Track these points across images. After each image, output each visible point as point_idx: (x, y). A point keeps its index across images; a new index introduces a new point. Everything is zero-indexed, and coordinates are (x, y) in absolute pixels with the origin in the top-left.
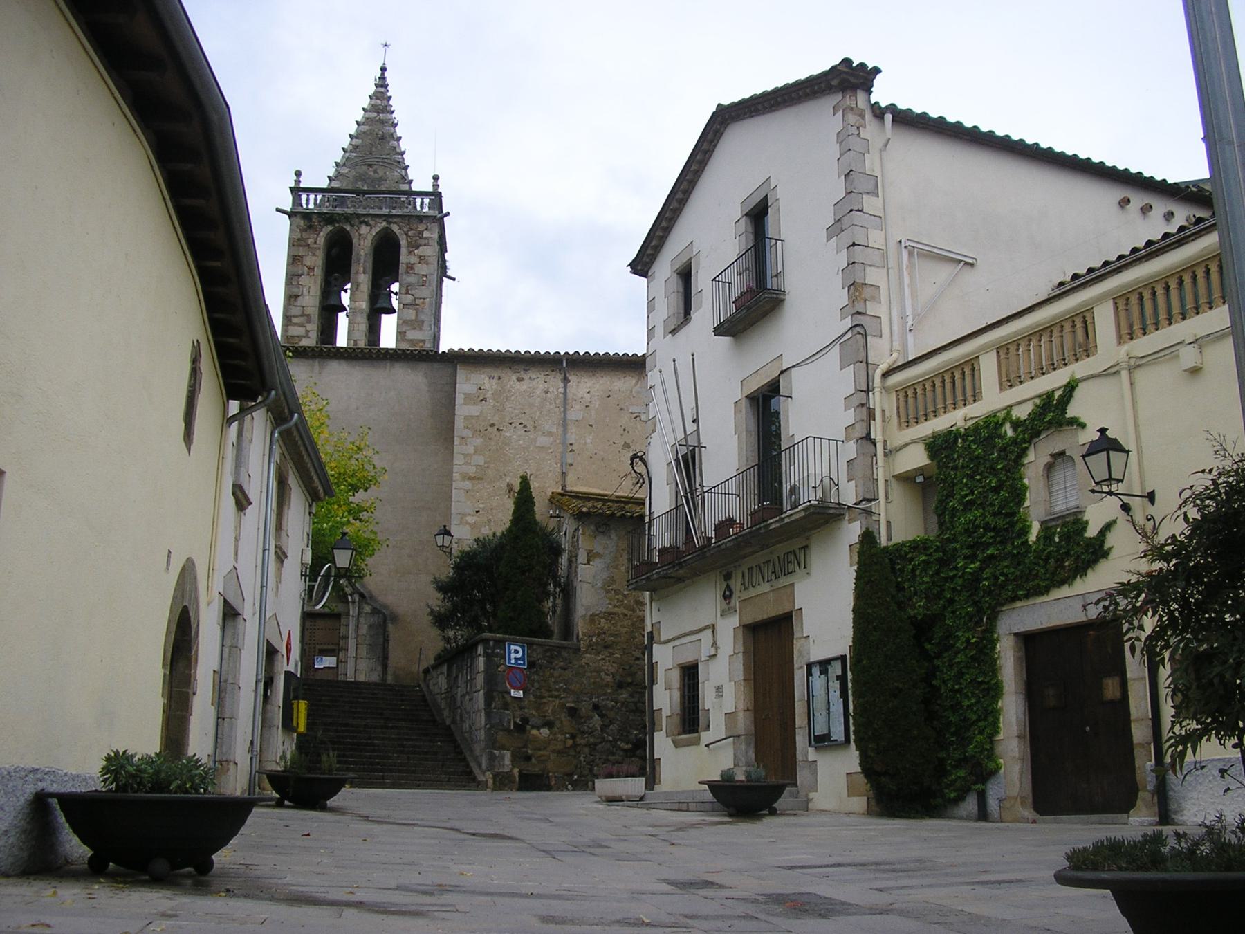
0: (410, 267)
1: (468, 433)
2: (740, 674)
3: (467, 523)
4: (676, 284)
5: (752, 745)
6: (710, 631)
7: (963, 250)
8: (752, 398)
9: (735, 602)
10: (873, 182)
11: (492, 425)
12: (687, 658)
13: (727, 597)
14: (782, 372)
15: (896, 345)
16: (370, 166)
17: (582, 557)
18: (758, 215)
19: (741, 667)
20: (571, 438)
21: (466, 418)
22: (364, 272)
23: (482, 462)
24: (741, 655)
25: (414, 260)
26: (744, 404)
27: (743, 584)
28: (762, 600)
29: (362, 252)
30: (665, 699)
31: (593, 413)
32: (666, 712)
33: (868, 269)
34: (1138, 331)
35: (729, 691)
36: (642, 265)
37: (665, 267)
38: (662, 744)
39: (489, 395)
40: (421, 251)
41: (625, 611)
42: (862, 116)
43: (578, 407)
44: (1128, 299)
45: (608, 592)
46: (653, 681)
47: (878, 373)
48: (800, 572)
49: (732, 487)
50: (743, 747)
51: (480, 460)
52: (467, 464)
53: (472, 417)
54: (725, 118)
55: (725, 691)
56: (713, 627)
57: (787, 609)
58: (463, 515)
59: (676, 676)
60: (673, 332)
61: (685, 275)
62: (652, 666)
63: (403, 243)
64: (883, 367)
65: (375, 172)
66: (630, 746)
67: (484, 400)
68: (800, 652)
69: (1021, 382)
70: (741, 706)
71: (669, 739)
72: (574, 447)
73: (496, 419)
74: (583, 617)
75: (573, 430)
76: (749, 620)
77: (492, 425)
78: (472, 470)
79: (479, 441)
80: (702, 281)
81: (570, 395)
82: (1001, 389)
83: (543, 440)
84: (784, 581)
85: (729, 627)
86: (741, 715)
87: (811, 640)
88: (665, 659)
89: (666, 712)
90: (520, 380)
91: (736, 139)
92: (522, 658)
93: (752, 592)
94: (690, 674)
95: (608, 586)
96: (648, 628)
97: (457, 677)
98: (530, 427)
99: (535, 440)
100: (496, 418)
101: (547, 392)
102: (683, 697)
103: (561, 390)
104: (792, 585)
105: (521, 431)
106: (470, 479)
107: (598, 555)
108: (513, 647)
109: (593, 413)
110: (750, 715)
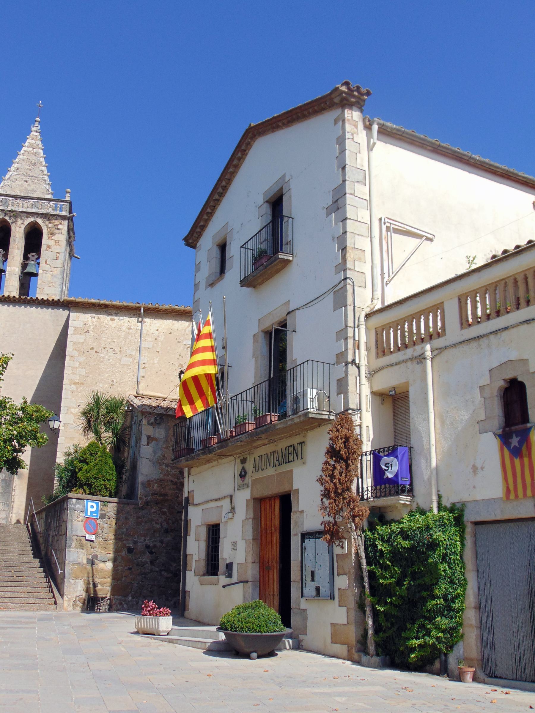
0: (49, 247)
1: (76, 353)
2: (250, 535)
3: (72, 413)
4: (216, 253)
5: (258, 589)
6: (228, 500)
7: (425, 228)
8: (268, 333)
9: (248, 480)
10: (362, 174)
11: (92, 349)
12: (213, 520)
13: (243, 475)
14: (289, 313)
15: (378, 294)
16: (26, 181)
17: (144, 440)
18: (276, 203)
19: (251, 530)
20: (143, 360)
21: (75, 343)
22: (18, 249)
23: (84, 373)
24: (251, 521)
25: (51, 242)
26: (261, 336)
27: (254, 467)
28: (269, 478)
29: (17, 236)
30: (195, 547)
31: (160, 343)
32: (195, 558)
33: (356, 236)
34: (523, 302)
35: (242, 546)
36: (192, 240)
37: (208, 241)
38: (193, 581)
39: (90, 329)
40: (55, 237)
41: (172, 479)
42: (356, 127)
43: (149, 339)
44: (496, 286)
45: (160, 465)
46: (187, 533)
47: (363, 314)
48: (298, 462)
49: (250, 396)
50: (250, 590)
51: (83, 371)
52: (73, 373)
53: (79, 343)
54: (253, 133)
55: (238, 546)
56: (231, 497)
57: (204, 376)
58: (69, 408)
59: (203, 532)
60: (212, 285)
61: (223, 248)
62: (187, 522)
63: (45, 231)
64: (367, 310)
65: (29, 185)
66: (170, 575)
67: (88, 332)
68: (296, 523)
69: (508, 312)
70: (250, 560)
71: (197, 578)
72: (146, 366)
73: (95, 345)
74: (143, 484)
75: (144, 353)
76: (258, 495)
77: (92, 349)
78: (77, 378)
79: (82, 359)
80: (234, 251)
81: (144, 331)
82: (462, 328)
83: (126, 360)
84: (286, 468)
85: (243, 497)
86: (250, 566)
87: (305, 514)
88: (197, 518)
89: (195, 558)
90: (112, 320)
91: (263, 149)
92: (96, 512)
93: (261, 475)
94: (214, 532)
95: (159, 462)
96: (186, 494)
97: (51, 522)
98: (117, 351)
99: (120, 360)
100: (95, 344)
101: (130, 329)
102: (208, 546)
103: (140, 328)
104: (291, 471)
105: (111, 353)
106: (75, 384)
107: (155, 439)
108: (90, 504)
109: (160, 343)
110: (257, 567)
